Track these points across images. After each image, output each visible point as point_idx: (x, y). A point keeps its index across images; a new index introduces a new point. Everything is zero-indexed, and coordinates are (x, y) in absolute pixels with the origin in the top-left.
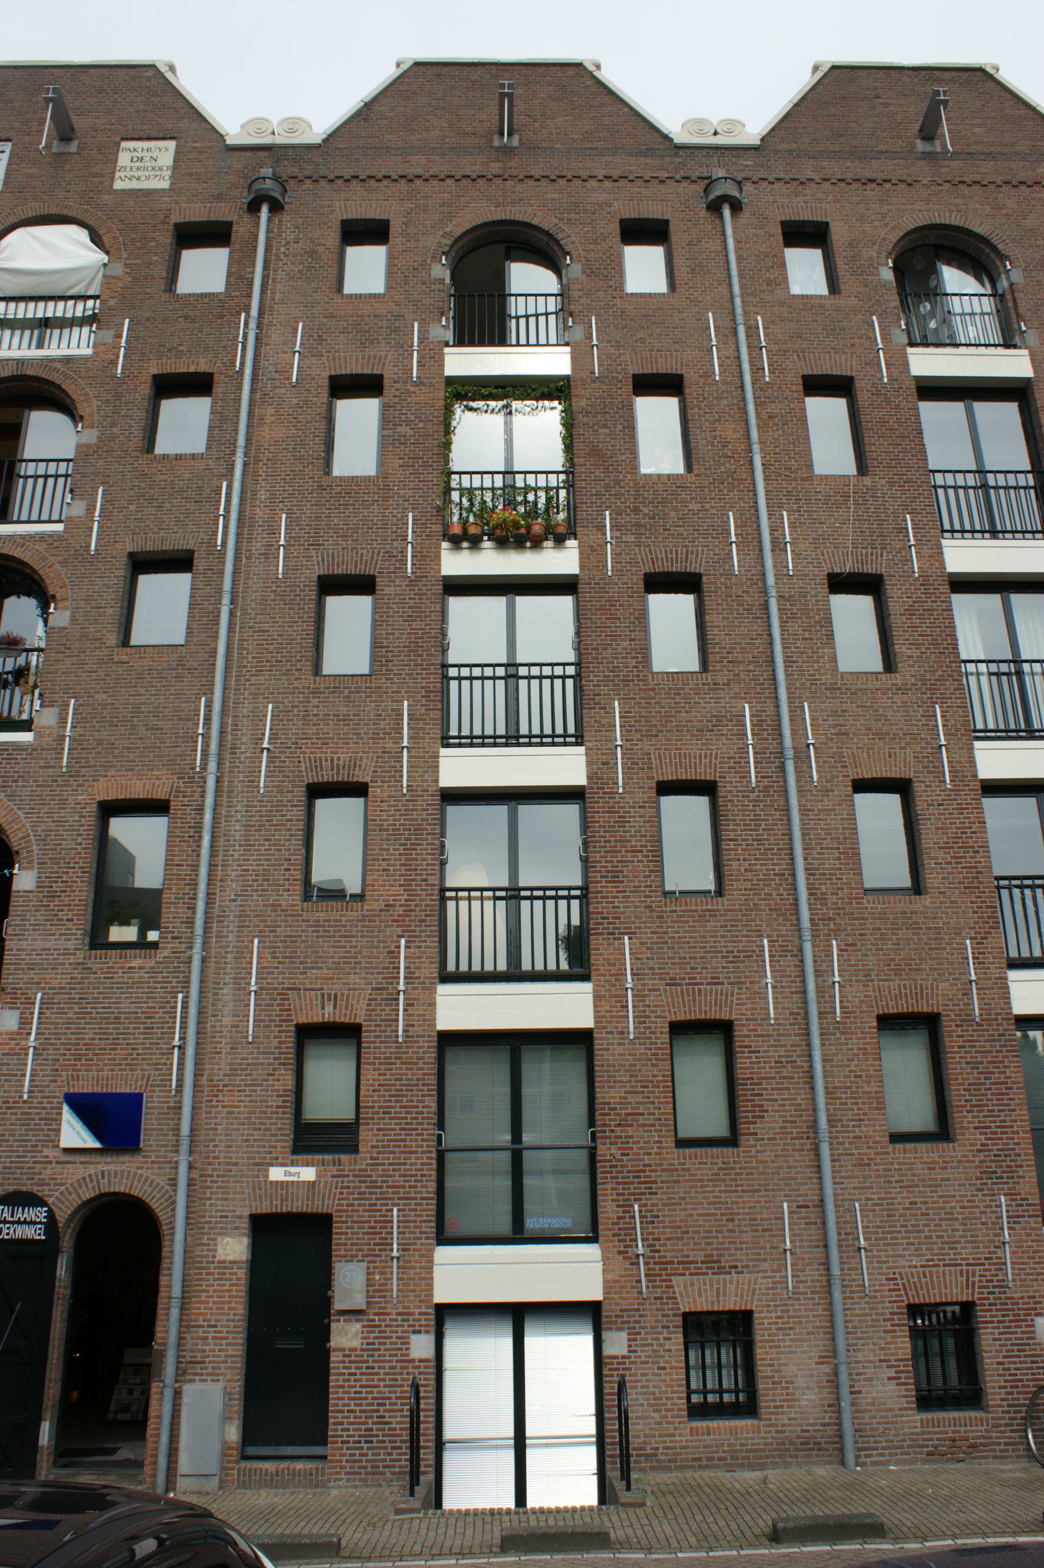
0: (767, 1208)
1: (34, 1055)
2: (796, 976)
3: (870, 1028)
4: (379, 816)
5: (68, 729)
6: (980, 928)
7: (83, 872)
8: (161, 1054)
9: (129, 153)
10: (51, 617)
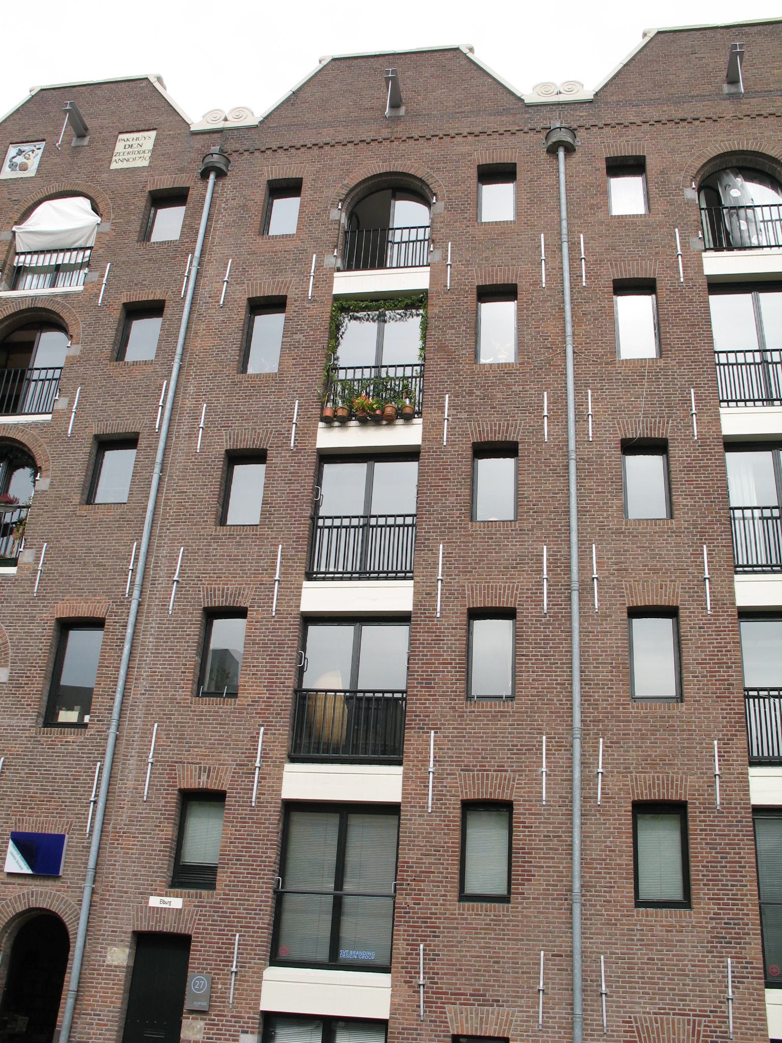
0: (528, 955)
3: (625, 811)
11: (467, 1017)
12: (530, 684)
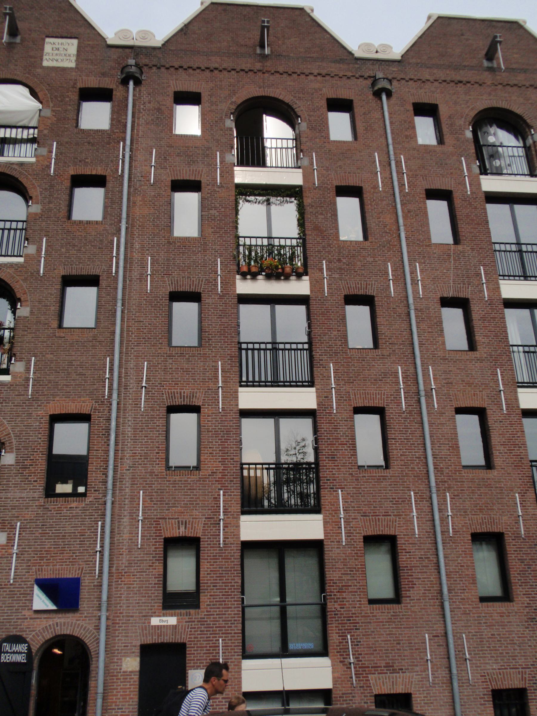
0: (417, 637)
1: (16, 557)
2: (429, 512)
3: (467, 540)
4: (207, 424)
5: (32, 374)
6: (523, 487)
7: (42, 454)
8: (89, 555)
9: (51, 45)
10: (18, 311)
11: (383, 682)
12: (399, 457)
